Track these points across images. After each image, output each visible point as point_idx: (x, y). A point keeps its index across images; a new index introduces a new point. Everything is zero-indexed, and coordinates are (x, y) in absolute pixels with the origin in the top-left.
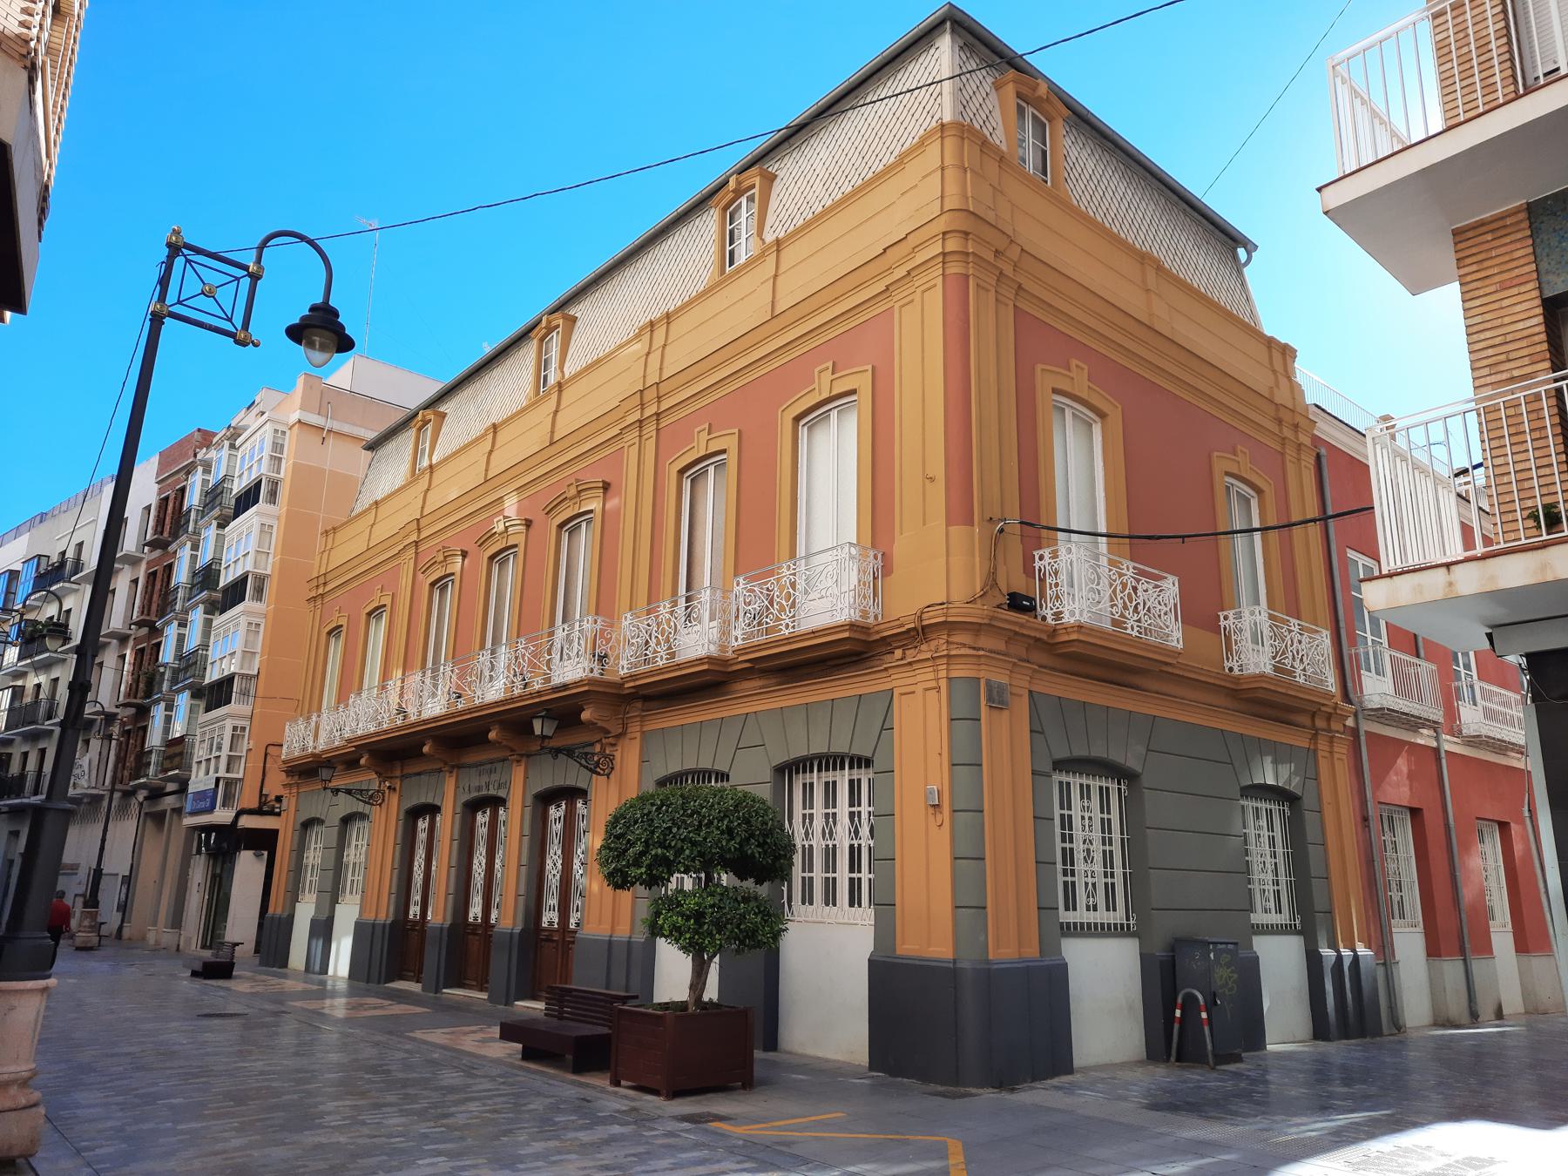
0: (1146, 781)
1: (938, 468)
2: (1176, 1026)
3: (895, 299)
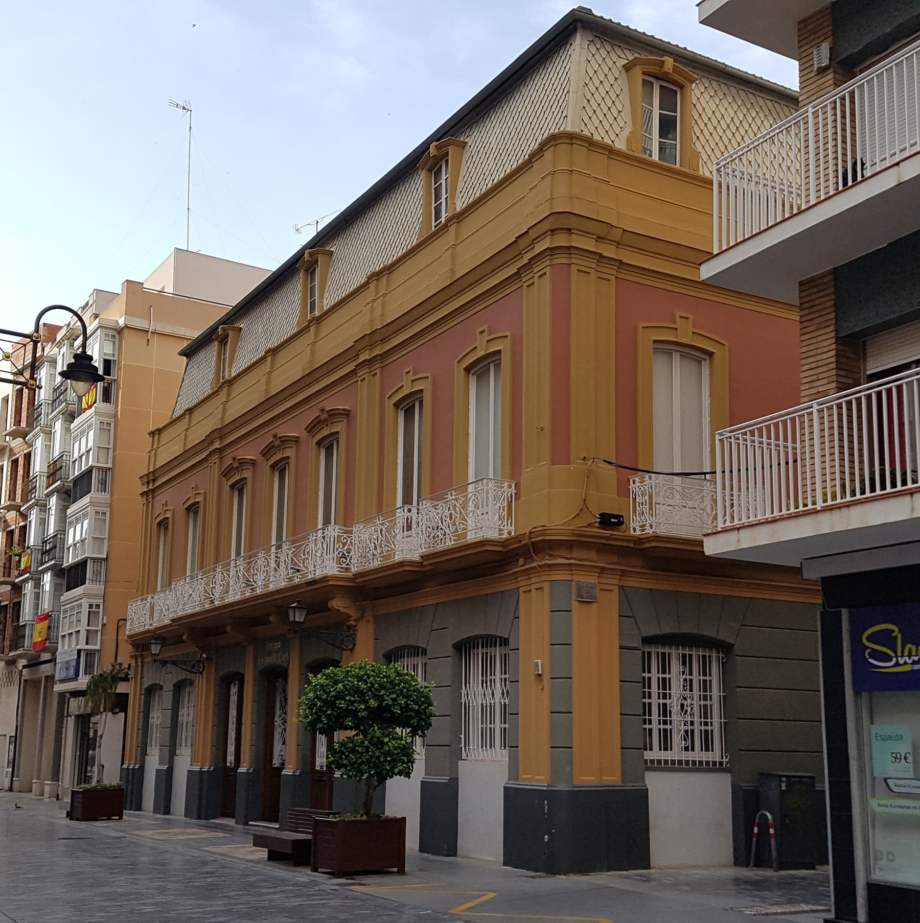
0: (738, 650)
1: (546, 423)
2: (754, 840)
3: (524, 280)
